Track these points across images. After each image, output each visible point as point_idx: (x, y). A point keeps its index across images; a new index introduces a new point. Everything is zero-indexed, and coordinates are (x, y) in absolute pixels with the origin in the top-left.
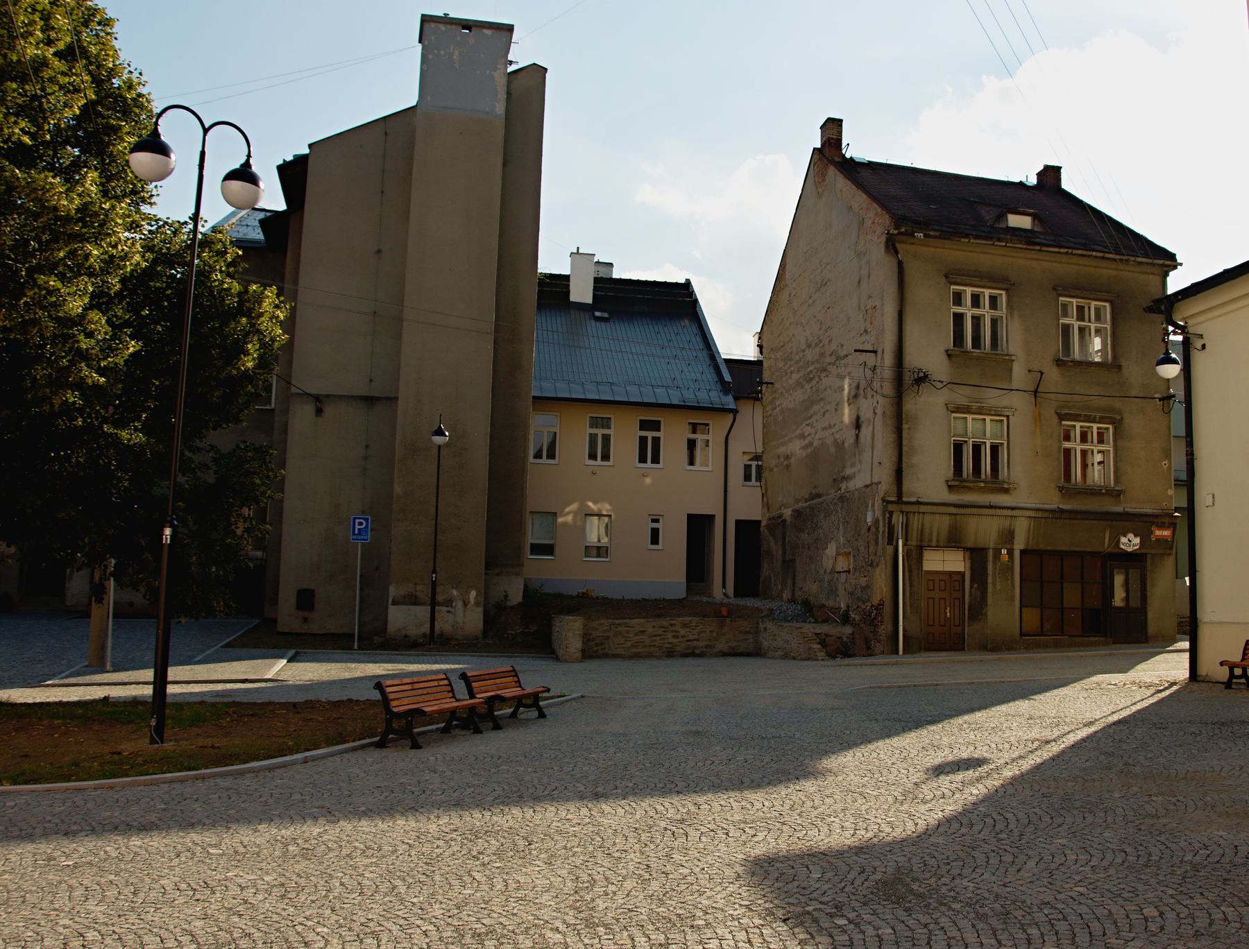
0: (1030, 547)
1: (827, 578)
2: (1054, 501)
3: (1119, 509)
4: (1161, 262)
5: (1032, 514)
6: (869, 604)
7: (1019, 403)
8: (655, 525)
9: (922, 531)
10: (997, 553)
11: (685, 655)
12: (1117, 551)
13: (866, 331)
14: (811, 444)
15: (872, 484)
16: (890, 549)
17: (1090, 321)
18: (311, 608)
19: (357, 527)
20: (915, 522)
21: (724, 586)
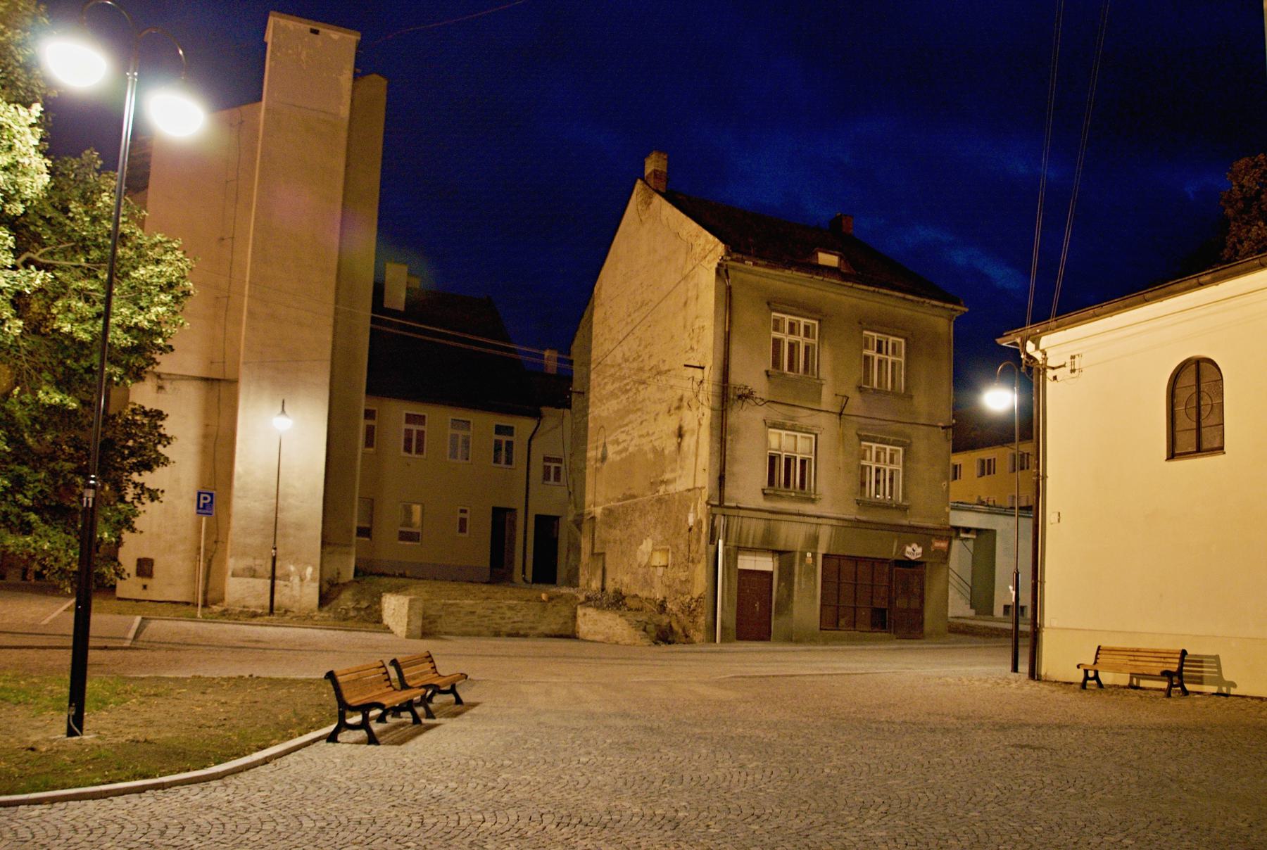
0: (831, 553)
1: (641, 571)
2: (852, 513)
3: (905, 522)
4: (951, 306)
5: (834, 522)
6: (689, 597)
7: (825, 423)
8: (463, 515)
9: (740, 534)
10: (803, 556)
11: (509, 635)
12: (903, 558)
13: (692, 348)
14: (626, 449)
15: (695, 488)
16: (712, 548)
17: (887, 353)
18: (150, 575)
19: (202, 501)
20: (735, 523)
21: (524, 573)
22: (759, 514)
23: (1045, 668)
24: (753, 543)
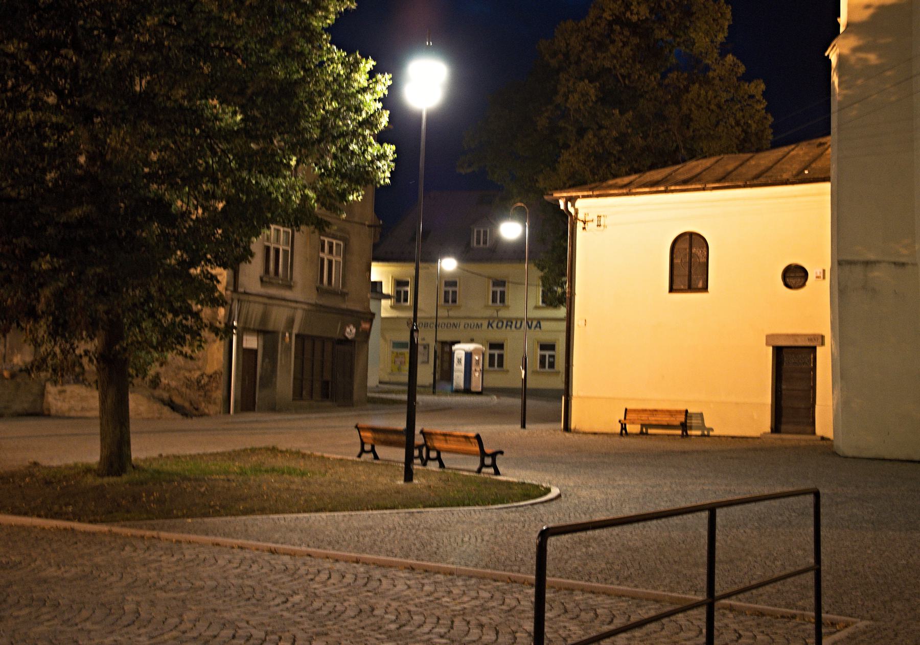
2: (313, 298)
5: (306, 307)
10: (284, 335)
12: (343, 338)
22: (260, 299)
23: (573, 425)
24: (254, 325)
